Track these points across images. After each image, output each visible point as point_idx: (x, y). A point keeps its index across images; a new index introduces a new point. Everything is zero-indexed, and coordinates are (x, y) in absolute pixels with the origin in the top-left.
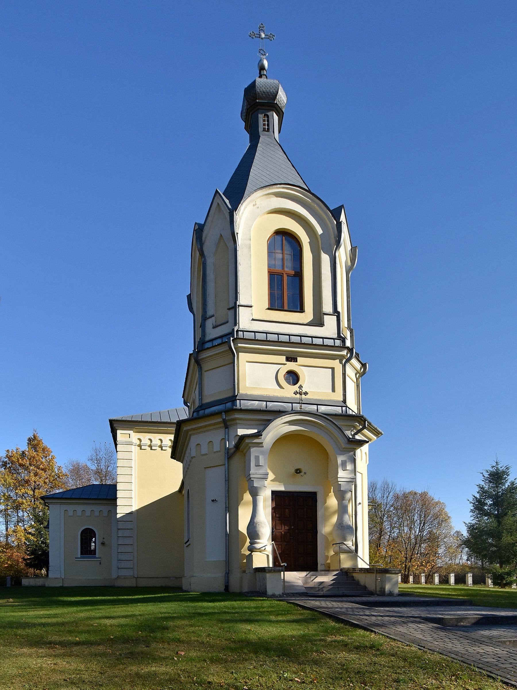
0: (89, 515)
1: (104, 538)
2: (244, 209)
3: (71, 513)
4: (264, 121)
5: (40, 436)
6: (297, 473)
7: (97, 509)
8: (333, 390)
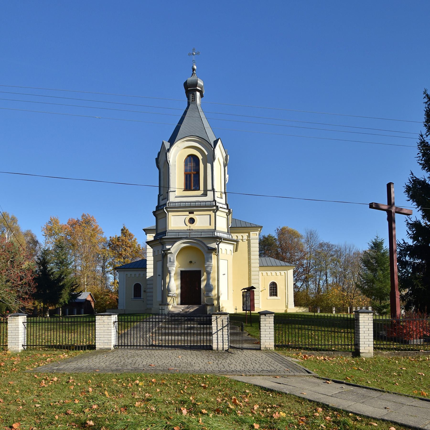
0: (134, 276)
1: (145, 288)
2: (173, 150)
3: (129, 276)
4: (193, 97)
5: (127, 228)
6: (190, 263)
7: (137, 273)
8: (210, 225)
